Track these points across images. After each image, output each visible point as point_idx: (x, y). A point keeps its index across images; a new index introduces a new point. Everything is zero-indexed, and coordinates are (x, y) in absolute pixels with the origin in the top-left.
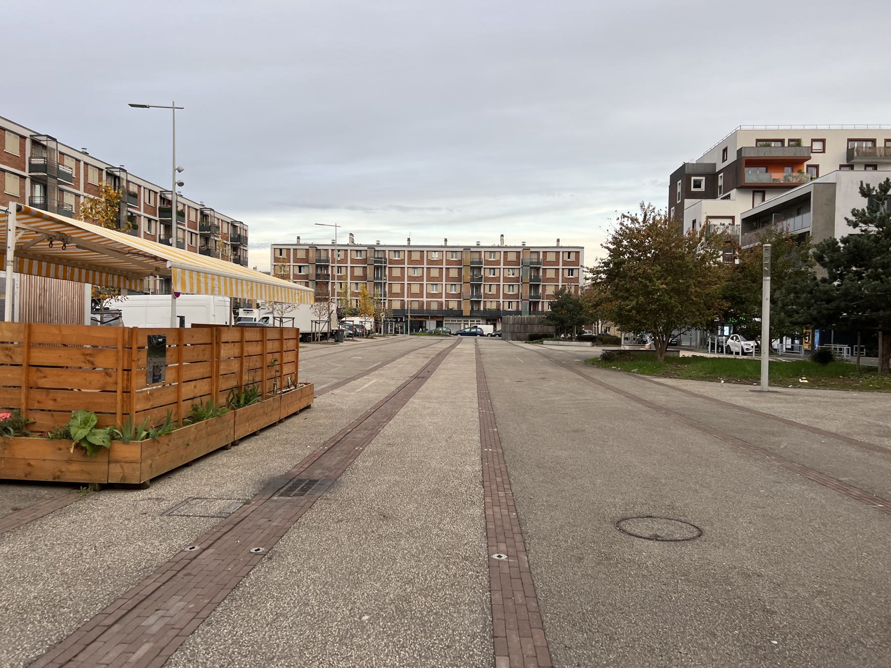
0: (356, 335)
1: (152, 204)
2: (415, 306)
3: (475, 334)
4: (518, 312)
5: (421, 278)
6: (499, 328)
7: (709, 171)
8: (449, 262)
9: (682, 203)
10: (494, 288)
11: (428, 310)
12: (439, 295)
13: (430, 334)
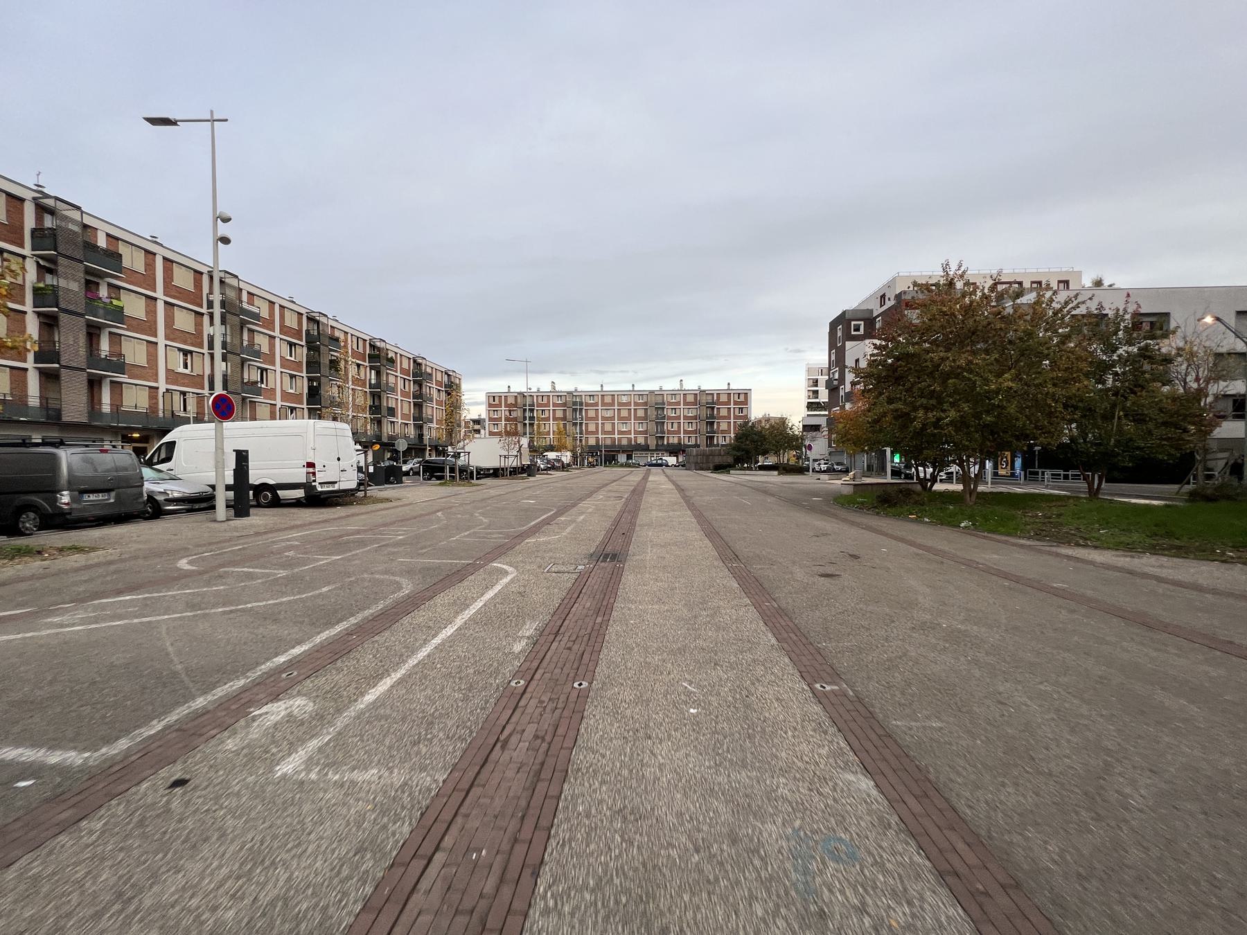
0: (553, 468)
1: (361, 350)
2: (609, 442)
3: (661, 465)
4: (697, 446)
5: (612, 418)
6: (681, 459)
7: (867, 316)
8: (636, 404)
9: (844, 346)
10: (675, 426)
11: (620, 446)
12: (629, 432)
13: (622, 466)
